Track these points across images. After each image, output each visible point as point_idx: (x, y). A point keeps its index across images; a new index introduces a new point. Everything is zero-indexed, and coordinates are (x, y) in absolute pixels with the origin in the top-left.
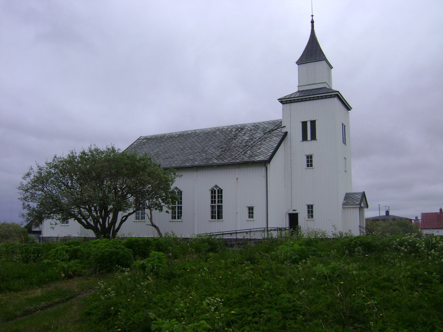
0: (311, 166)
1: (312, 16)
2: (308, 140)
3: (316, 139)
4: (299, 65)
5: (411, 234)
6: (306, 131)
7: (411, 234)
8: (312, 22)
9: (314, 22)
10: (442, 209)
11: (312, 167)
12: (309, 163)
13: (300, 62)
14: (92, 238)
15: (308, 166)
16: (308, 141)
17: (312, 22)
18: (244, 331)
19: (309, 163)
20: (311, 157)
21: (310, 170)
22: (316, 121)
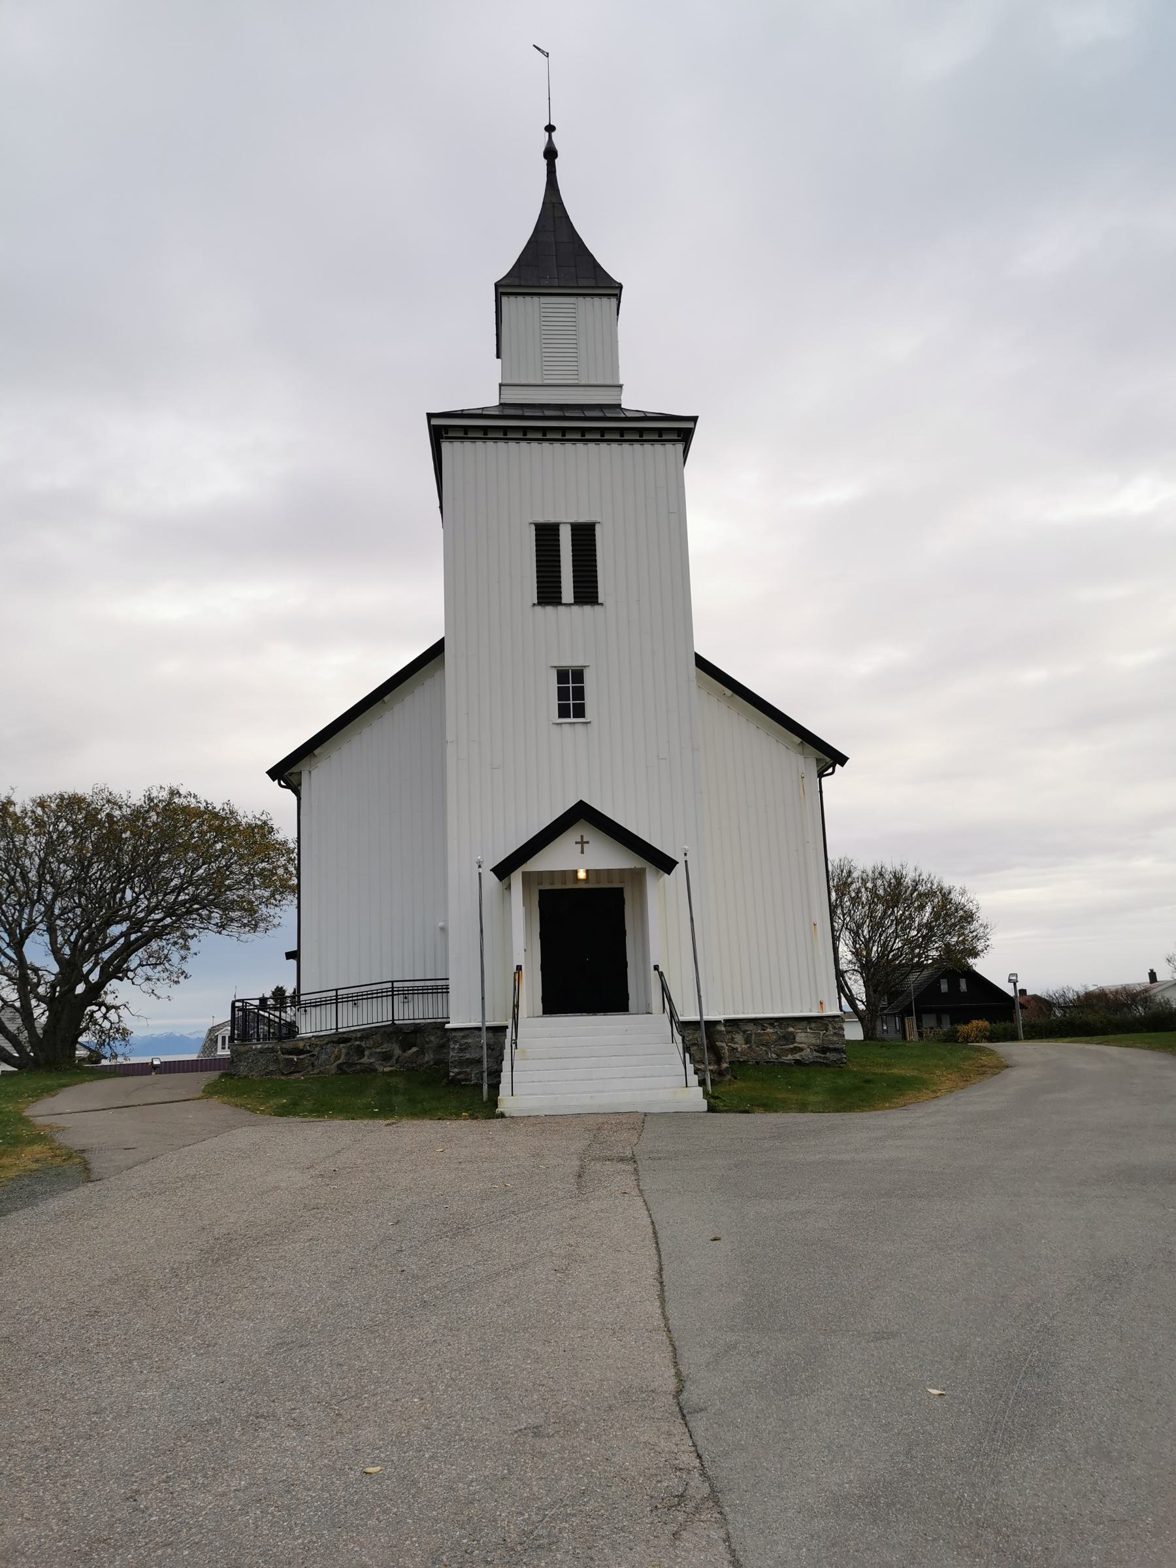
0: (580, 712)
1: (550, 129)
2: (564, 601)
3: (597, 602)
4: (504, 407)
5: (337, 1031)
6: (555, 535)
7: (337, 1031)
8: (551, 154)
9: (502, 1071)
10: (1155, 973)
11: (583, 716)
12: (571, 685)
13: (503, 289)
14: (678, 1117)
15: (563, 712)
16: (566, 605)
17: (551, 154)
18: (1175, 1006)
19: (571, 702)
20: (578, 675)
21: (571, 730)
22: (598, 527)
